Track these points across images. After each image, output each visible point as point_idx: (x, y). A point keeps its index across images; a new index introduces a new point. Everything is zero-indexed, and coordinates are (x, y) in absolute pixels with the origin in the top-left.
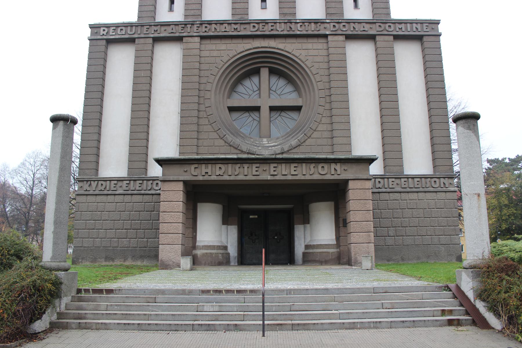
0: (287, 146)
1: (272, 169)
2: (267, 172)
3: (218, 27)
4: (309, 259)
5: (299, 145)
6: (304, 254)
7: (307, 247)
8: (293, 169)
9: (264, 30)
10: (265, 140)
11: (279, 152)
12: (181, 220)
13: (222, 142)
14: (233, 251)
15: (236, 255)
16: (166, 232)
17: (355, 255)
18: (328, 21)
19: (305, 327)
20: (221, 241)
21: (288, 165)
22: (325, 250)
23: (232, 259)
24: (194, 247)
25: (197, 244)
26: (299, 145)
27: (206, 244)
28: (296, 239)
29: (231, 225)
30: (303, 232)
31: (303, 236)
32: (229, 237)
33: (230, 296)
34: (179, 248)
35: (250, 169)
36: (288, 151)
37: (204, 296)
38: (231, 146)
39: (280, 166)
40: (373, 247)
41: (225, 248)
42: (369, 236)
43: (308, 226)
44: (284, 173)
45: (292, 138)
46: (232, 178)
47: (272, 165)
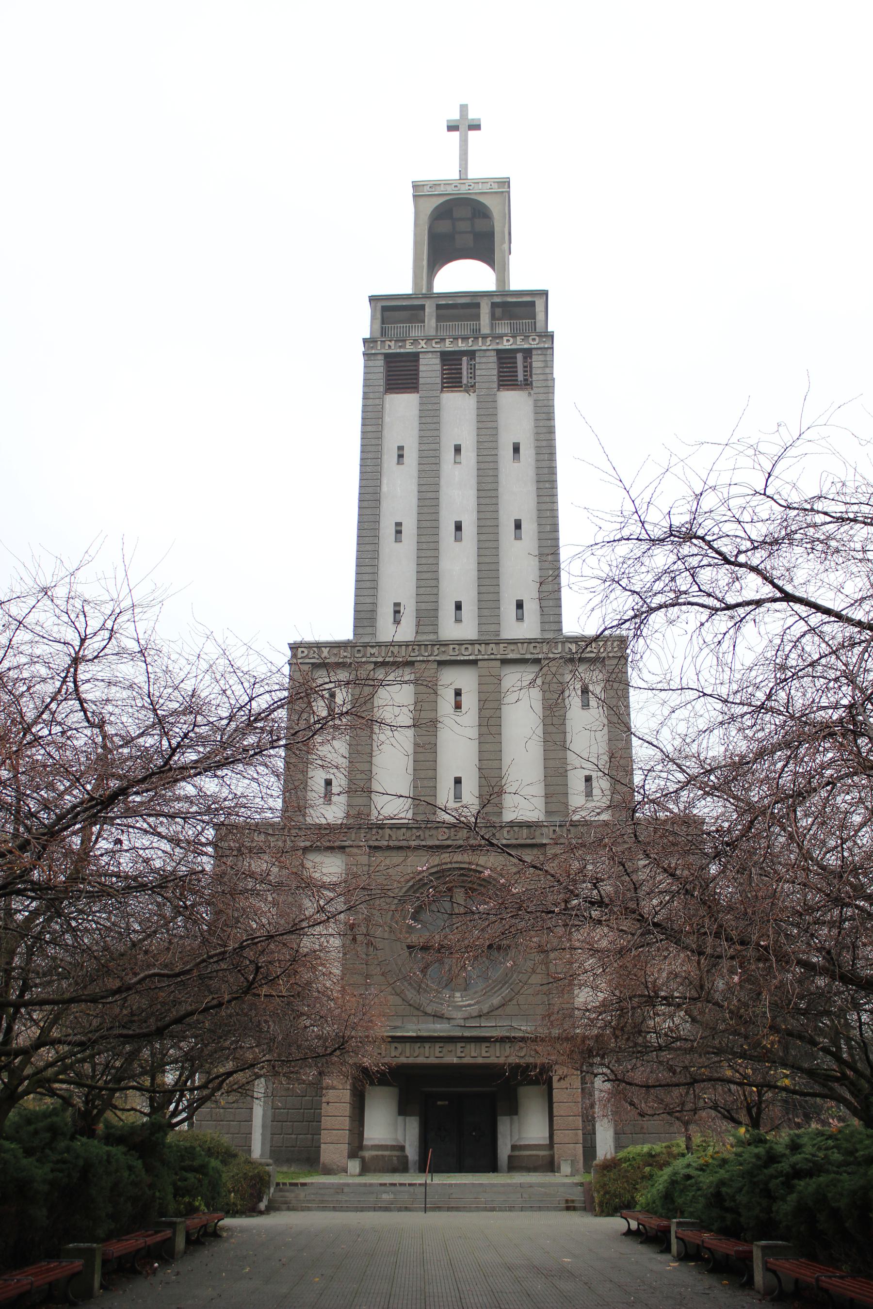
0: (487, 1006)
1: (459, 1050)
2: (453, 1053)
3: (393, 833)
4: (515, 1165)
5: (503, 1005)
6: (510, 1157)
7: (514, 1148)
8: (484, 1049)
9: (457, 837)
10: (458, 994)
11: (476, 1014)
12: (347, 1113)
13: (398, 1000)
14: (412, 1152)
15: (417, 1158)
16: (329, 1127)
17: (559, 1158)
18: (545, 824)
19: (457, 1209)
20: (396, 1139)
21: (478, 1044)
22: (534, 1153)
23: (410, 1165)
24: (361, 1147)
25: (365, 1143)
26: (503, 1005)
27: (376, 1142)
28: (499, 1136)
29: (410, 1116)
30: (509, 1126)
31: (509, 1132)
32: (407, 1132)
33: (402, 1188)
34: (344, 1148)
35: (432, 1049)
36: (488, 1013)
37: (383, 1188)
38: (410, 1005)
39: (468, 1046)
40: (581, 1149)
41: (402, 1148)
42: (576, 1134)
43: (515, 1117)
44: (473, 1054)
45: (495, 992)
46: (411, 1060)
47: (459, 1045)
